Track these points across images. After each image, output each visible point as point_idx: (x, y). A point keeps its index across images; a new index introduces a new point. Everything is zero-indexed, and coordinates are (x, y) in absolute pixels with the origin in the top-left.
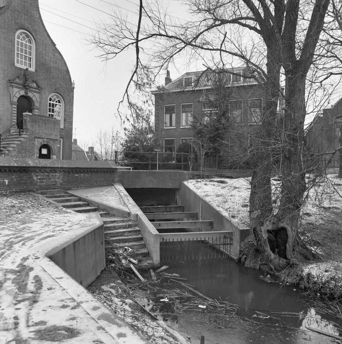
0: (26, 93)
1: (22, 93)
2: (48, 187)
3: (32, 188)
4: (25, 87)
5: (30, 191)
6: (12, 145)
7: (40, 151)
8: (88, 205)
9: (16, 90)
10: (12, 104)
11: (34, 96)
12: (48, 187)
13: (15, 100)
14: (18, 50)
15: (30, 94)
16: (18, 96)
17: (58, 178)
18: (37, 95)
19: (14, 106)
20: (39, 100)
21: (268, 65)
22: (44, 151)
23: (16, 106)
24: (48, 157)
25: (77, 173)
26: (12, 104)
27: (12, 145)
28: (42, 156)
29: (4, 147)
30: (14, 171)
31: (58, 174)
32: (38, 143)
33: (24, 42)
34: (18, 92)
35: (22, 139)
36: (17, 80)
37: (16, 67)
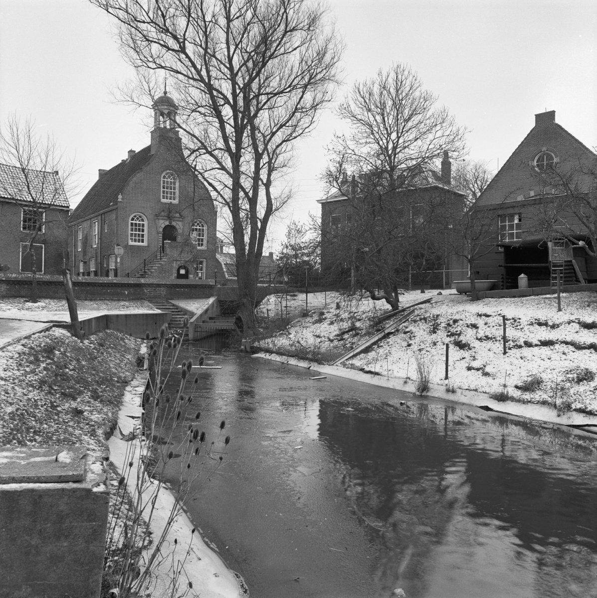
0: (170, 223)
1: (167, 223)
2: (155, 297)
3: (144, 297)
4: (169, 218)
5: (142, 299)
6: (154, 268)
7: (178, 271)
8: (177, 309)
9: (162, 221)
10: (158, 233)
11: (179, 225)
12: (155, 297)
13: (161, 230)
14: (164, 188)
15: (174, 223)
16: (163, 226)
17: (163, 291)
18: (180, 223)
19: (160, 235)
20: (182, 227)
21: (235, 230)
22: (182, 272)
23: (161, 235)
24: (186, 276)
25: (178, 288)
26: (158, 233)
27: (154, 268)
28: (179, 276)
29: (148, 269)
30: (119, 286)
31: (162, 289)
32: (175, 265)
33: (169, 180)
34: (163, 223)
35: (162, 263)
36: (163, 213)
37: (162, 203)
